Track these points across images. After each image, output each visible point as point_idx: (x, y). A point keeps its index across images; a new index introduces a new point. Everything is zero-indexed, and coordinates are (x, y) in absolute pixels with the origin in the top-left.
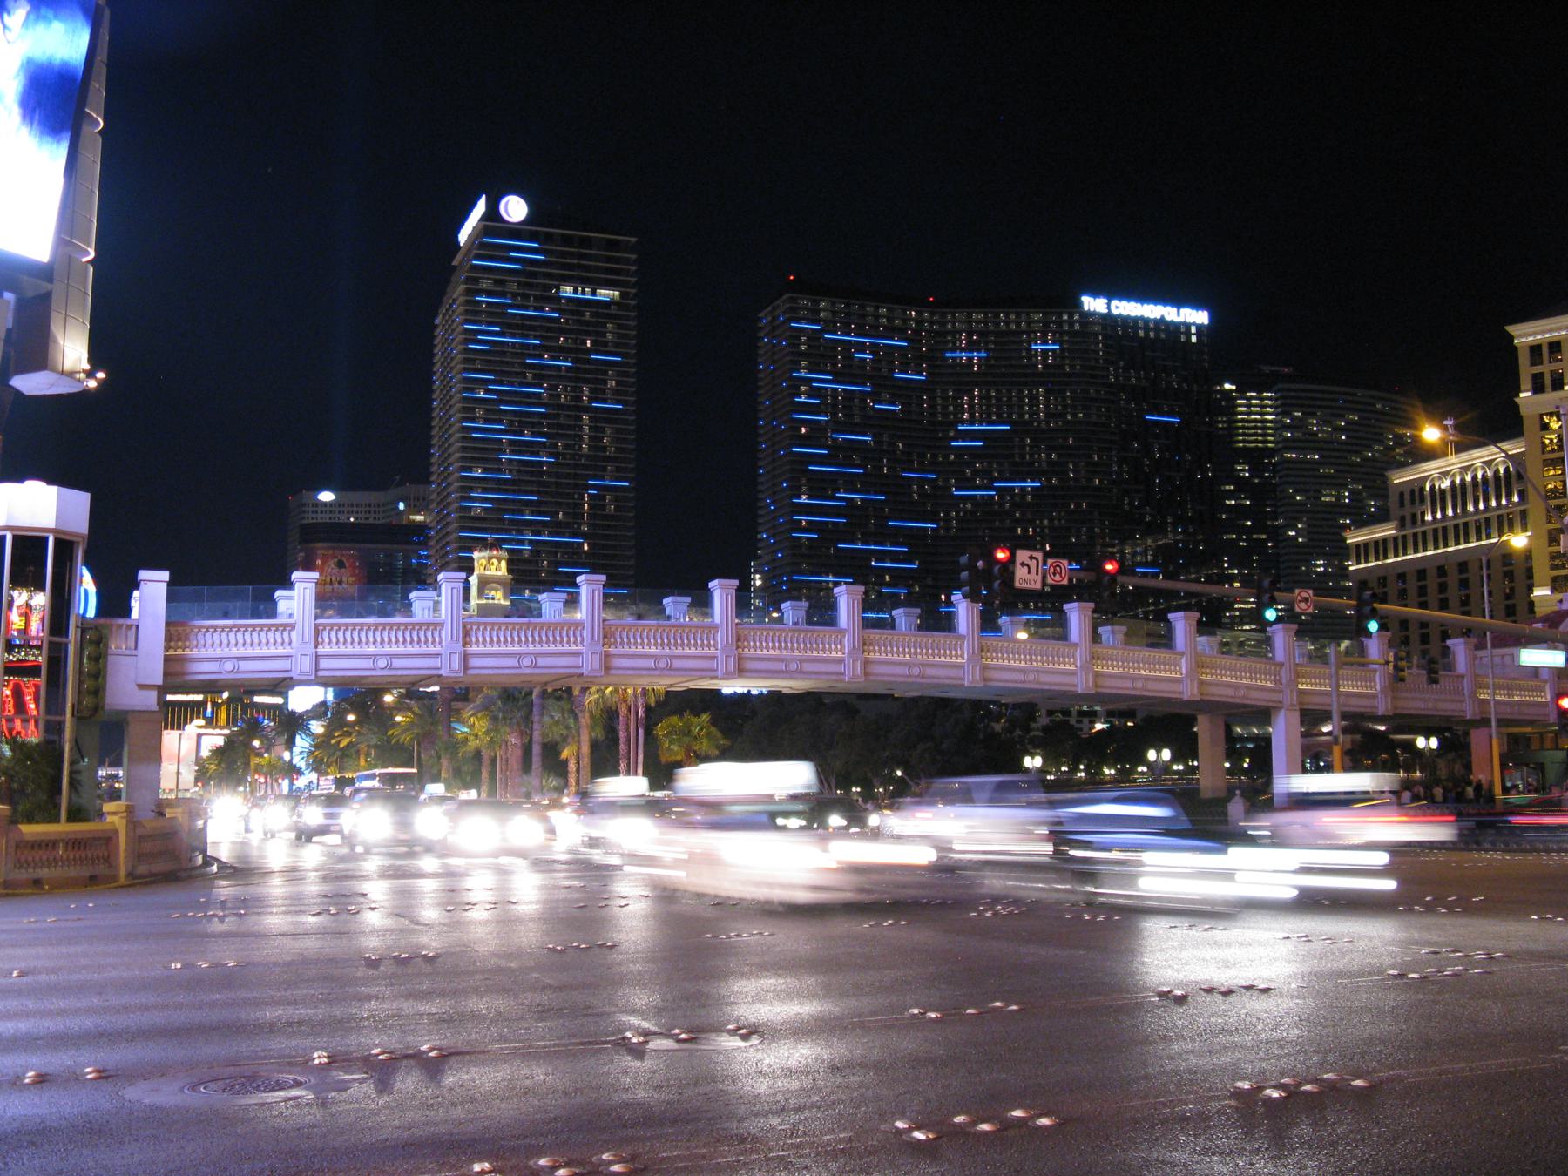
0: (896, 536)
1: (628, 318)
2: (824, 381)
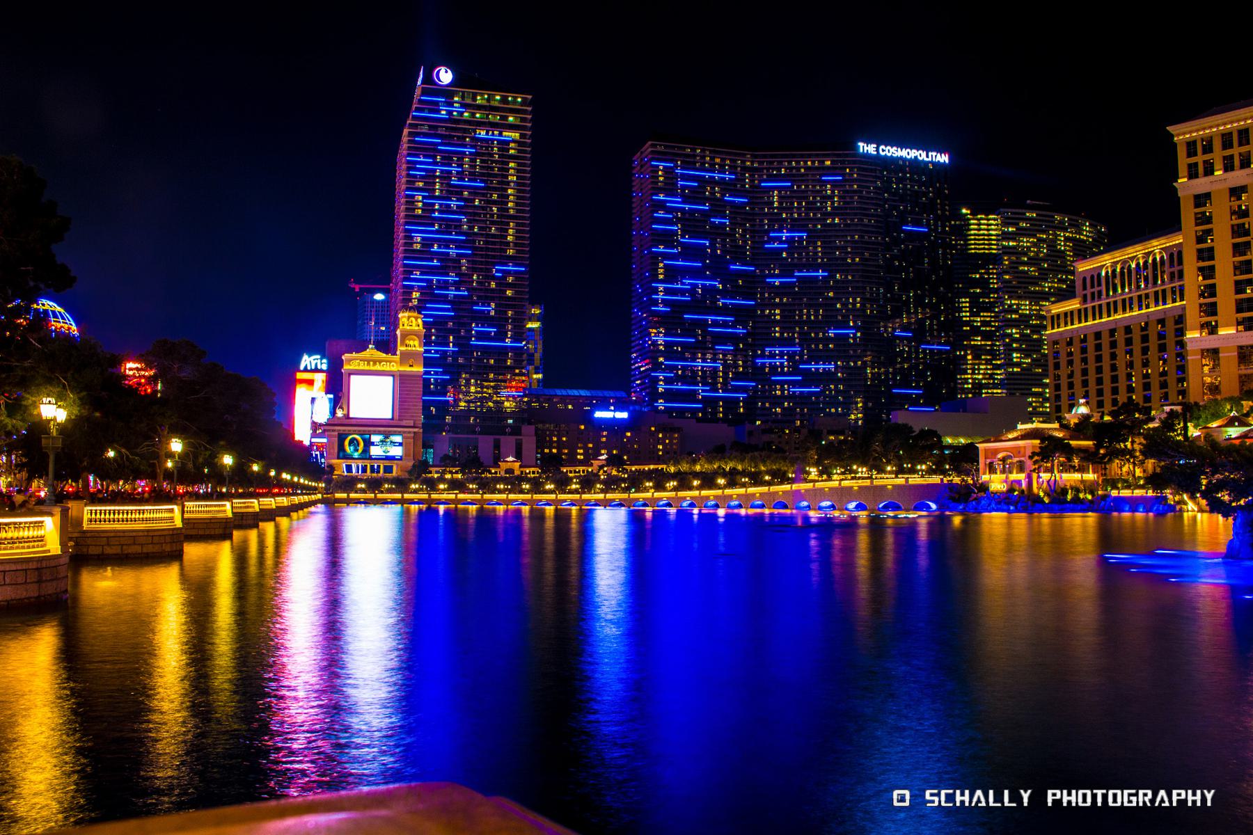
0: (725, 311)
1: (525, 158)
2: (675, 202)
